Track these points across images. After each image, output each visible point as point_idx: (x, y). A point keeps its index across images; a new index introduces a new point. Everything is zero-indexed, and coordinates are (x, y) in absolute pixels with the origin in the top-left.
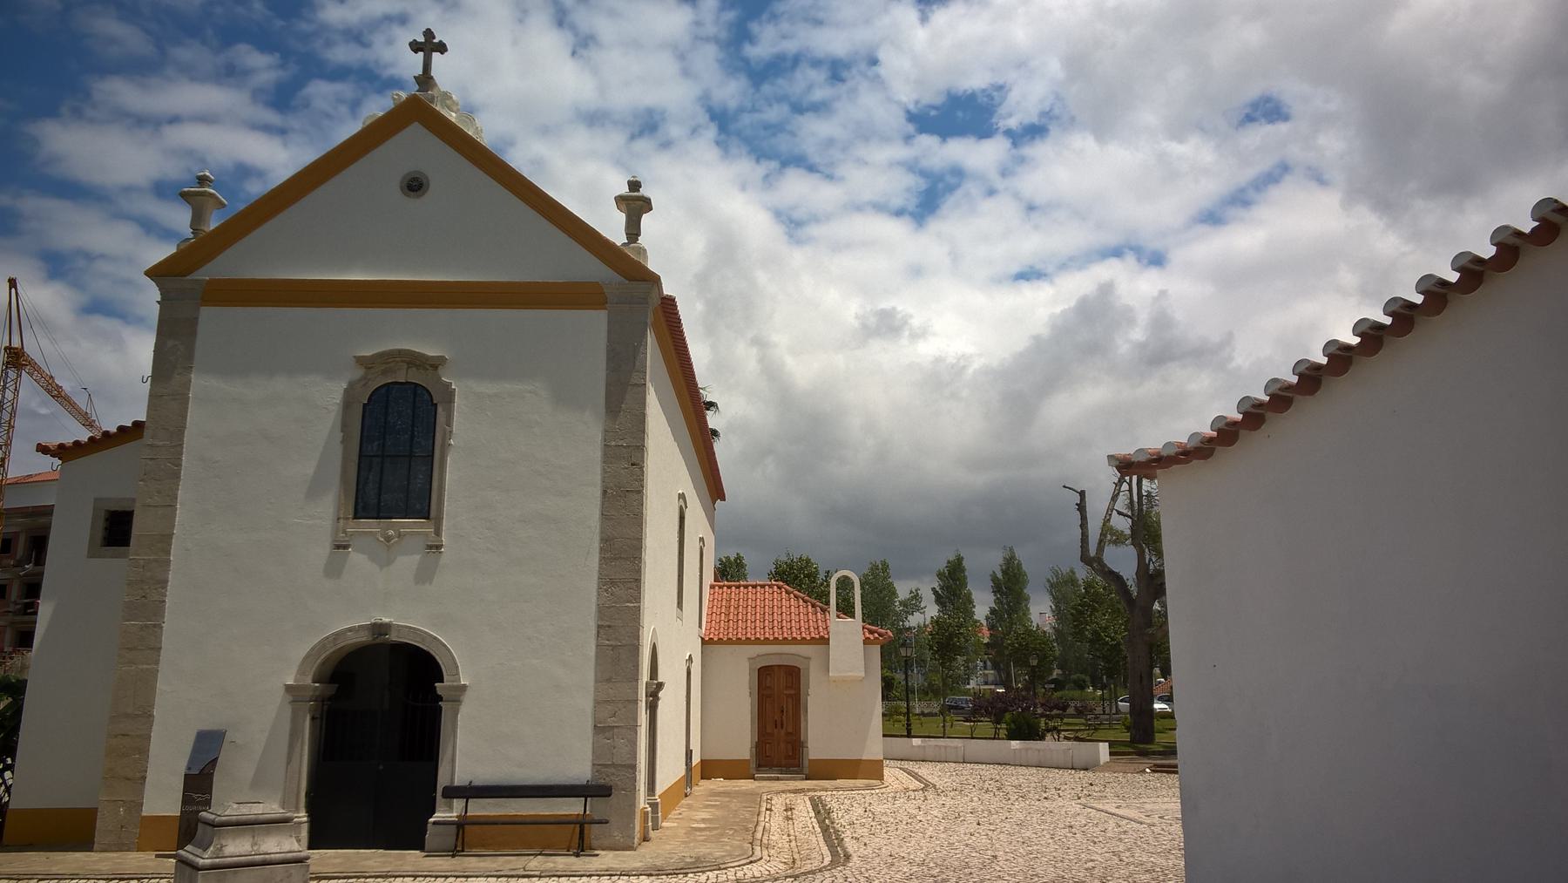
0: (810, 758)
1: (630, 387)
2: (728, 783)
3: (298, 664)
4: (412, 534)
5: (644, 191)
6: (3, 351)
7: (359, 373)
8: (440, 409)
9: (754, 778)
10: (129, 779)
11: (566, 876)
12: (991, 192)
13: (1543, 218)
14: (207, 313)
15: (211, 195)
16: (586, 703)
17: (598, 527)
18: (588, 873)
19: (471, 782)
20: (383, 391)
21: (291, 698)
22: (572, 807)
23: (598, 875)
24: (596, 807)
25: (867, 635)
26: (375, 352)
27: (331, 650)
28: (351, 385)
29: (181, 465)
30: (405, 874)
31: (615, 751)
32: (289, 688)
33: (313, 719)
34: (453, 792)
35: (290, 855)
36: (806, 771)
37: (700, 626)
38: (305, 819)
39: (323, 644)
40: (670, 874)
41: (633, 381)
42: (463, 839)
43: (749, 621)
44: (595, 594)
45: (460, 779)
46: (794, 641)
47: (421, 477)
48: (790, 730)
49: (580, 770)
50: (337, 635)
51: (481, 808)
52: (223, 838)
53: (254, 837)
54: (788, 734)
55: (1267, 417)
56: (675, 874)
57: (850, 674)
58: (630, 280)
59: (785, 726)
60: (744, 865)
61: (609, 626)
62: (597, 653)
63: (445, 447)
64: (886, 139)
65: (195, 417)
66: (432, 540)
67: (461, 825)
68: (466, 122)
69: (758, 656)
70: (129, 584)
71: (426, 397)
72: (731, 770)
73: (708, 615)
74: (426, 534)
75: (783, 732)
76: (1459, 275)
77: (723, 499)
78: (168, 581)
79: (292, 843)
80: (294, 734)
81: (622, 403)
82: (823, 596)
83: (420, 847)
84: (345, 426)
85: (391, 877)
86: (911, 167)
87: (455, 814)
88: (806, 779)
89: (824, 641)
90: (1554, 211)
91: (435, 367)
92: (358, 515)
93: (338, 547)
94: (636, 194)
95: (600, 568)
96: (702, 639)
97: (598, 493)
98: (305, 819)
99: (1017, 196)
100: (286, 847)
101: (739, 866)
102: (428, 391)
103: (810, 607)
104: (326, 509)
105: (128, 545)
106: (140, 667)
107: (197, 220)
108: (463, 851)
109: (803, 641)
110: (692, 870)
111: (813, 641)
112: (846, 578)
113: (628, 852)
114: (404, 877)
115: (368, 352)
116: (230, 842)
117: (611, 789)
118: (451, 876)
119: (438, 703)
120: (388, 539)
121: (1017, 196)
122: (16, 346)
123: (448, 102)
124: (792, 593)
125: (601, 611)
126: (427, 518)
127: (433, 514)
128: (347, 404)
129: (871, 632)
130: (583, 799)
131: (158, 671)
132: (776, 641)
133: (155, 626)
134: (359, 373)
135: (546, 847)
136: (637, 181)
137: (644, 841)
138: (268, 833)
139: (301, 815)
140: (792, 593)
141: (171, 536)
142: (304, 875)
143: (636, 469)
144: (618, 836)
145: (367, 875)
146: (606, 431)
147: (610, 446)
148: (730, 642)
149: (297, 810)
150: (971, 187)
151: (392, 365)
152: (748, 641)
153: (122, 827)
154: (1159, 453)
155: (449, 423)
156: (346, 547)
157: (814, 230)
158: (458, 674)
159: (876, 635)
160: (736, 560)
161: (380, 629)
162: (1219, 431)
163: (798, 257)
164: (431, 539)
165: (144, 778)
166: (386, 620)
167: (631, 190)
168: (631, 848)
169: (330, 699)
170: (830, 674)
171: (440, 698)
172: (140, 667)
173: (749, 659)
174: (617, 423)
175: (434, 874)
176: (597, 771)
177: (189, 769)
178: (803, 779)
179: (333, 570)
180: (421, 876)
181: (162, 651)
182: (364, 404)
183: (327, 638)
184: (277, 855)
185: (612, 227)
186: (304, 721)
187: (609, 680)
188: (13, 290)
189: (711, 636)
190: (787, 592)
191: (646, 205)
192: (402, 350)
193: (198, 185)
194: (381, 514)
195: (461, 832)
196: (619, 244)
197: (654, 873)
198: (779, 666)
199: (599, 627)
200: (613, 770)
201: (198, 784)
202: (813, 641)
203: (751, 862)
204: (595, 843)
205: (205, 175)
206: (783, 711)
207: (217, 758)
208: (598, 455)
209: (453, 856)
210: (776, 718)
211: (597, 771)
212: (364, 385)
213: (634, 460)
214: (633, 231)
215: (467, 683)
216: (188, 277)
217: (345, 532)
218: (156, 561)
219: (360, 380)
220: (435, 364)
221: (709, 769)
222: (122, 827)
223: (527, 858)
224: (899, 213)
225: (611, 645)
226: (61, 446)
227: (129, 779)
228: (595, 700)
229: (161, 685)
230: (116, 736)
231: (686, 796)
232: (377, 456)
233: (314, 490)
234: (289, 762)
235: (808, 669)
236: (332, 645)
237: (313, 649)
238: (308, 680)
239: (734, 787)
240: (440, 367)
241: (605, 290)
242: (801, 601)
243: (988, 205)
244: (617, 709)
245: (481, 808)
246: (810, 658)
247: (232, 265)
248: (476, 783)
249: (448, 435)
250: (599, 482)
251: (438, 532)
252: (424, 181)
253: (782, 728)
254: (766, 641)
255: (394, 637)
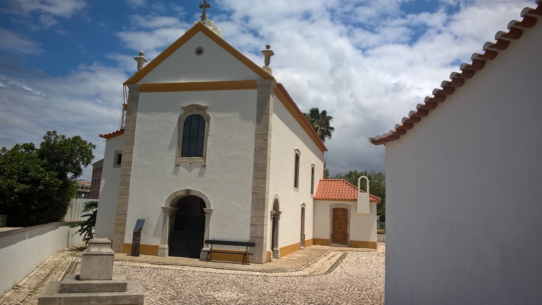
0: (351, 240)
1: (264, 115)
2: (167, 240)
3: (166, 200)
4: (198, 162)
5: (271, 49)
6: (122, 105)
7: (183, 112)
8: (206, 122)
9: (330, 246)
10: (121, 232)
11: (235, 270)
12: (439, 32)
13: (487, 50)
14: (141, 95)
15: (143, 58)
16: (248, 216)
17: (253, 160)
18: (241, 270)
19: (214, 239)
20: (190, 117)
21: (164, 211)
22: (243, 249)
23: (244, 270)
24: (250, 249)
25: (372, 199)
26: (187, 105)
27: (175, 197)
28: (181, 116)
29: (134, 141)
30: (188, 265)
31: (257, 232)
32: (163, 208)
33: (170, 217)
34: (208, 242)
35: (108, 253)
36: (349, 244)
37: (312, 192)
38: (168, 247)
39: (172, 195)
40: (266, 272)
41: (265, 112)
42: (211, 257)
43: (331, 193)
44: (252, 182)
45: (210, 238)
46: (345, 200)
47: (201, 144)
48: (344, 230)
49: (246, 237)
50: (176, 192)
51: (216, 247)
52: (91, 247)
53: (99, 247)
54: (343, 231)
55: (414, 125)
56: (268, 272)
57: (364, 212)
58: (265, 79)
59: (342, 229)
60: (293, 271)
61: (256, 192)
62: (252, 201)
63: (208, 134)
64: (395, 18)
65: (139, 127)
66: (203, 164)
67: (209, 252)
68: (215, 29)
69: (333, 204)
70: (121, 176)
71: (203, 119)
72: (323, 242)
73: (317, 190)
74: (202, 162)
75: (341, 231)
76: (462, 71)
77: (327, 151)
78: (131, 175)
79: (110, 250)
80: (164, 222)
81: (261, 120)
82: (355, 183)
83: (199, 258)
84: (179, 128)
85: (184, 266)
86: (408, 26)
87: (209, 249)
88: (349, 247)
89: (356, 200)
90: (489, 47)
91: (205, 109)
92: (183, 156)
93: (177, 166)
94: (268, 50)
95: (253, 174)
96: (313, 198)
97: (253, 149)
98: (168, 247)
99: (451, 33)
100: (108, 251)
101: (291, 272)
102: (203, 118)
103: (353, 188)
104: (174, 153)
105: (121, 164)
106: (124, 200)
107: (139, 65)
108: (211, 260)
109: (348, 200)
110: (280, 271)
111: (352, 200)
112: (363, 178)
113: (260, 265)
114: (188, 266)
115: (185, 106)
116: (92, 248)
117: (255, 244)
118: (201, 267)
119: (204, 214)
120: (191, 163)
121: (451, 33)
122: (126, 104)
123: (210, 23)
124: (347, 183)
125: (254, 187)
126: (202, 157)
127: (204, 155)
128: (179, 122)
129: (373, 198)
130: (211, 245)
131: (128, 201)
132: (339, 200)
133: (127, 188)
134: (183, 112)
135: (235, 261)
136: (268, 45)
137: (269, 262)
138: (103, 246)
139: (166, 246)
140: (347, 183)
141: (131, 162)
142: (112, 259)
143: (265, 141)
144: (257, 260)
145: (178, 264)
146: (256, 129)
147: (257, 134)
148: (323, 199)
149: (165, 244)
150: (431, 31)
151: (192, 109)
152: (329, 199)
153: (119, 246)
154: (374, 138)
155: (209, 127)
156: (179, 166)
157: (370, 52)
158: (210, 206)
159: (375, 199)
160: (354, 172)
161: (188, 191)
162: (397, 129)
163: (367, 62)
164: (203, 163)
165: (125, 232)
166: (190, 188)
167: (267, 48)
168: (261, 263)
169: (176, 212)
170: (358, 212)
171: (205, 213)
172: (124, 200)
173: (330, 205)
174: (260, 126)
175: (196, 266)
176: (251, 238)
177: (134, 230)
178: (347, 247)
179: (175, 172)
180: (193, 266)
181: (129, 196)
182: (184, 121)
183: (173, 193)
184: (105, 253)
185: (260, 62)
186: (167, 218)
187: (255, 210)
188: (124, 86)
189: (317, 197)
190: (346, 183)
191: (272, 53)
192: (195, 104)
193: (139, 55)
194: (189, 156)
195: (245, 256)
196: (261, 67)
197: (262, 271)
198: (340, 208)
199: (253, 192)
200: (256, 238)
201: (137, 234)
202: (352, 200)
203: (297, 271)
204: (250, 261)
205: (141, 52)
206: (341, 224)
207: (142, 228)
208: (253, 136)
209: (206, 261)
210: (339, 226)
211: (251, 238)
212: (184, 115)
213: (265, 138)
214: (267, 63)
215: (213, 209)
216: (136, 84)
217: (178, 161)
218: (127, 169)
219: (183, 114)
220: (205, 109)
221: (315, 241)
222: (119, 246)
223: (227, 263)
224: (404, 43)
225: (256, 199)
226: (106, 135)
227: (121, 232)
228: (251, 216)
229: (129, 206)
230: (117, 220)
231: (301, 249)
232: (188, 138)
233: (170, 147)
234: (163, 230)
235: (350, 210)
236: (175, 195)
237: (169, 196)
238: (168, 206)
239: (322, 248)
240: (206, 109)
241: (257, 83)
242: (350, 186)
243: (439, 37)
244: (258, 219)
245: (216, 247)
246: (351, 206)
247: (149, 80)
248: (215, 240)
249: (208, 130)
250: (254, 146)
251: (205, 162)
252: (202, 50)
253: (341, 229)
254: (335, 200)
255: (192, 194)
